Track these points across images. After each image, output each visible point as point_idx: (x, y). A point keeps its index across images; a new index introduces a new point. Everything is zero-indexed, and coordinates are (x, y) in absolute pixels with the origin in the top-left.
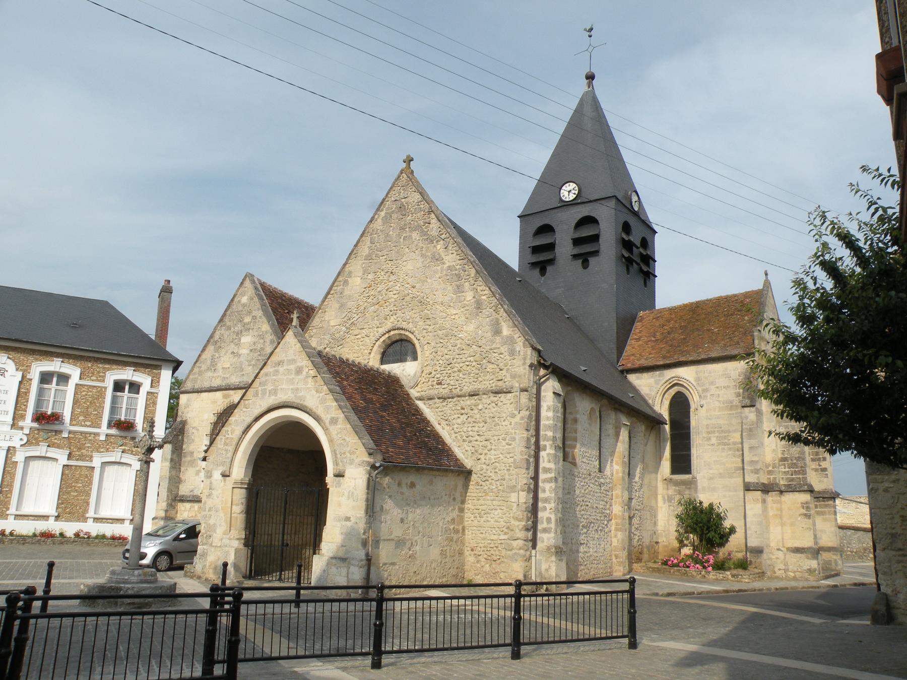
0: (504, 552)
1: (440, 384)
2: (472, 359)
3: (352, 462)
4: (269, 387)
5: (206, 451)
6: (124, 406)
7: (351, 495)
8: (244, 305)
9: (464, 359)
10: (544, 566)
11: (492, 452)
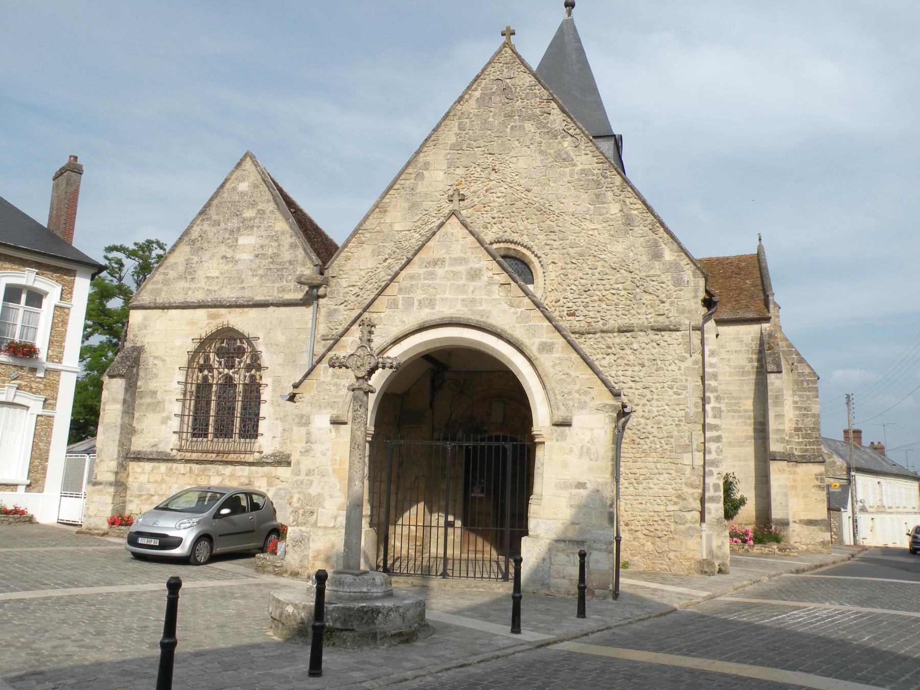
0: (672, 527)
1: (573, 315)
2: (621, 286)
3: (583, 406)
4: (419, 295)
5: (296, 386)
6: (19, 323)
7: (585, 452)
8: (243, 194)
9: (608, 286)
10: (715, 543)
11: (654, 403)
